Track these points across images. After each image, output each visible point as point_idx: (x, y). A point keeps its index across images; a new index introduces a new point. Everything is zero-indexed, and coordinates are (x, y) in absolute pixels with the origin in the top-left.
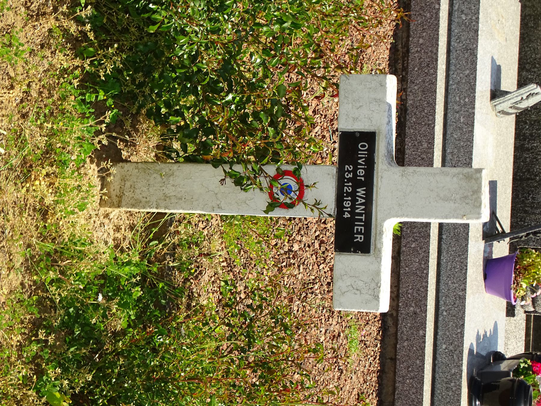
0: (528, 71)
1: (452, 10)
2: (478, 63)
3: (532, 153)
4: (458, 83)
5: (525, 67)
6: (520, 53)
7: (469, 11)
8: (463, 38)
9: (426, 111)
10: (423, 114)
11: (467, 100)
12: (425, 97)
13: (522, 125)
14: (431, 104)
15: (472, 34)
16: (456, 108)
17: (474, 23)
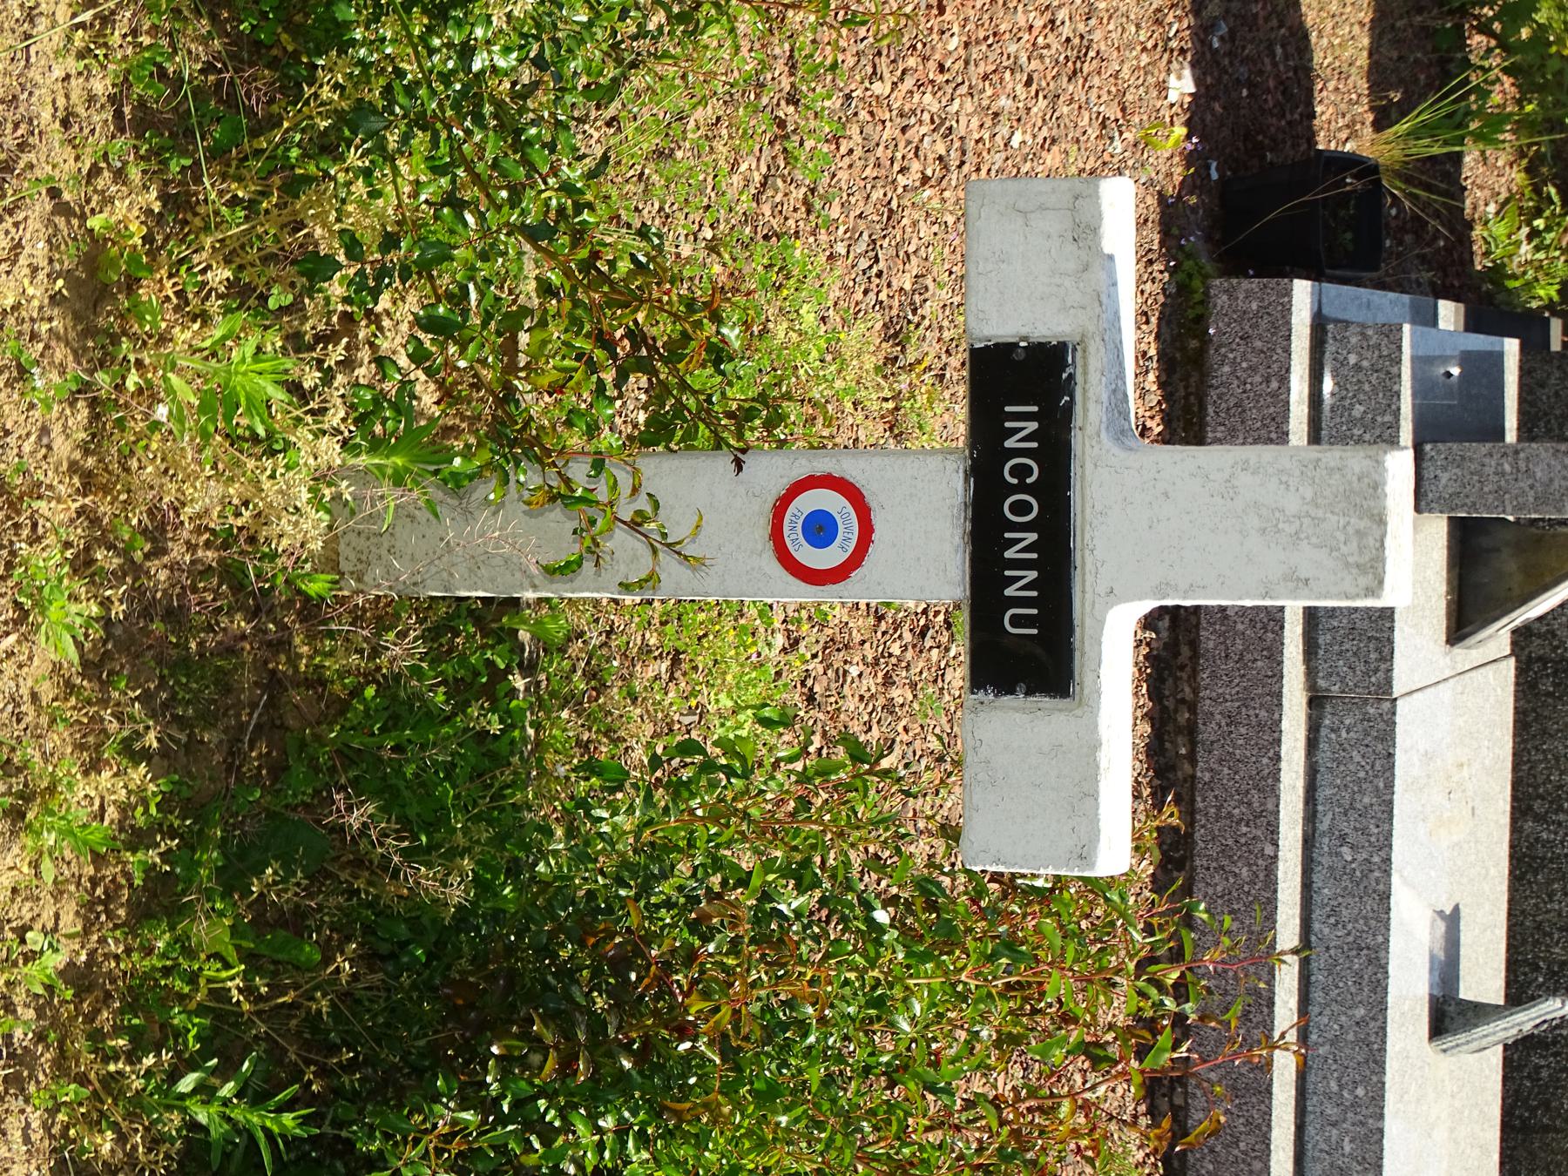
0: (1538, 818)
1: (1314, 831)
2: (1390, 989)
3: (1555, 1055)
4: (1334, 1042)
5: (1530, 808)
6: (1516, 767)
7: (1363, 840)
8: (1345, 912)
9: (1242, 1145)
10: (1236, 1152)
11: (1360, 1092)
12: (1239, 1106)
13: (1525, 974)
14: (1258, 1127)
15: (1370, 904)
16: (1331, 1110)
17: (1377, 874)
